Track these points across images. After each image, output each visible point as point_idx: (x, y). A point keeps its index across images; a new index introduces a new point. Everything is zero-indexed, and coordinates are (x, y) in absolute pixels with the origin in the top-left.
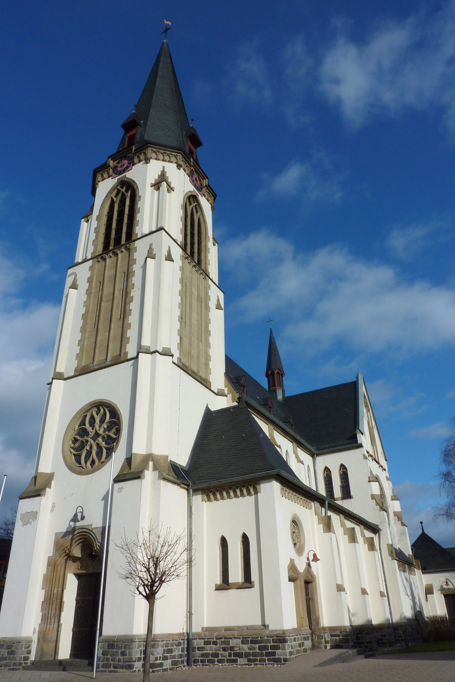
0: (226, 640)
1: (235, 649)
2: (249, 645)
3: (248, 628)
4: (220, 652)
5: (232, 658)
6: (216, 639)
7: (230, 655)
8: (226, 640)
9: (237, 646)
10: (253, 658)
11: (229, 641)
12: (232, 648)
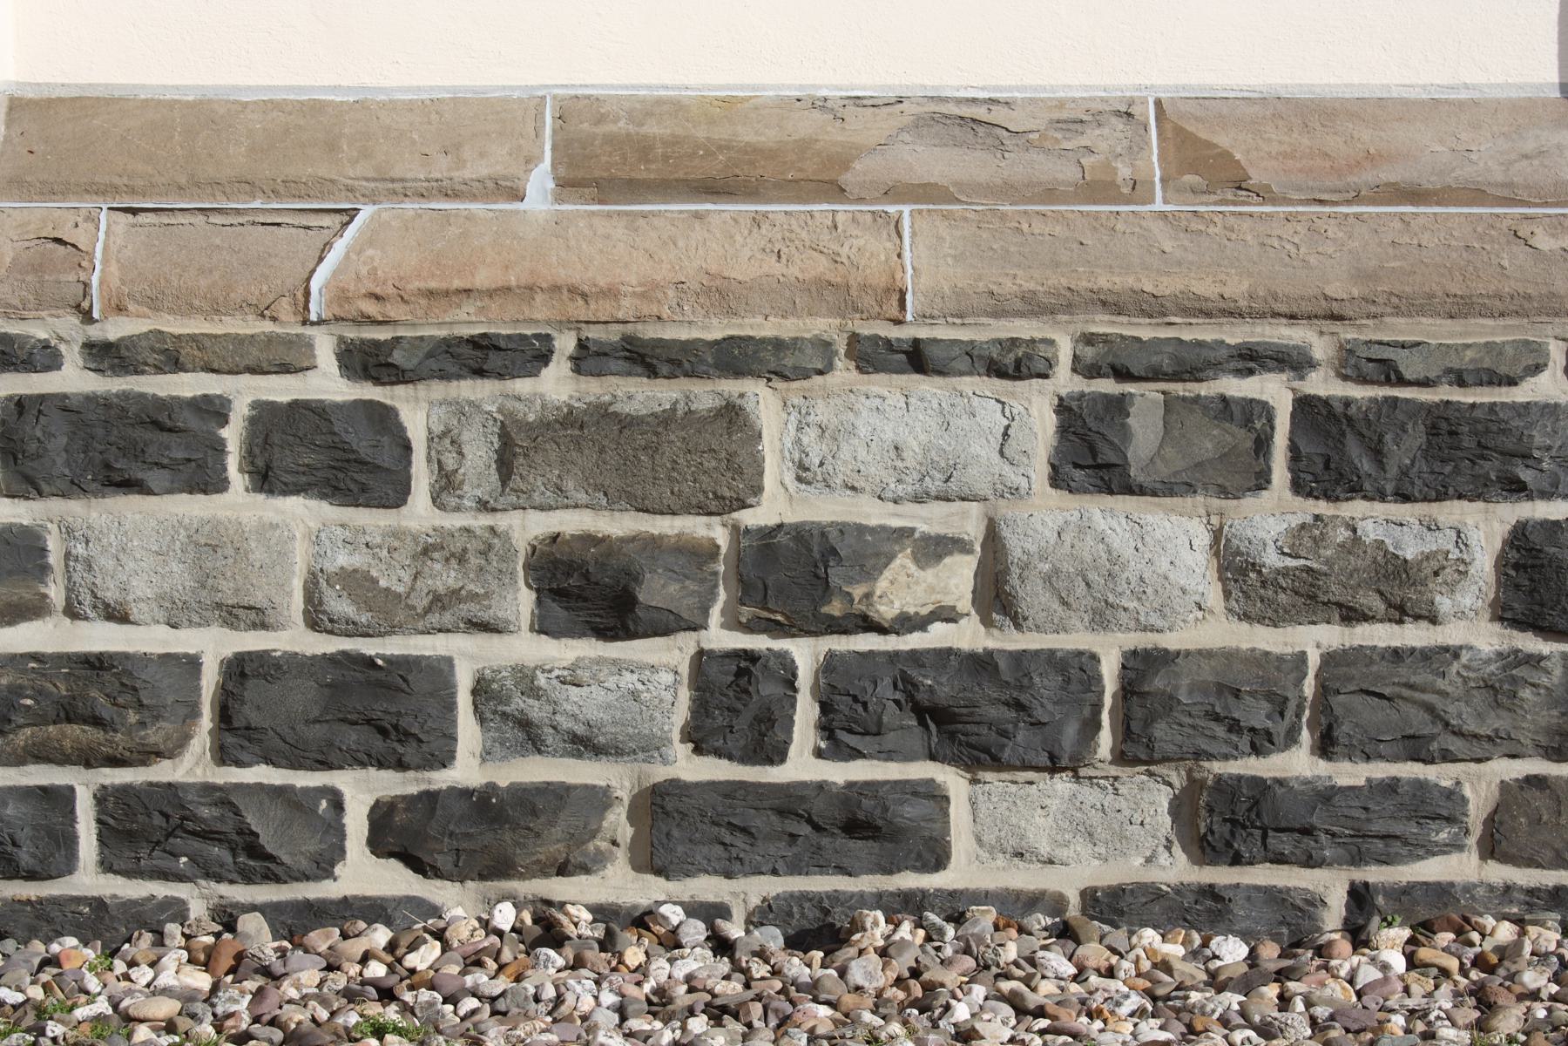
0: (642, 395)
1: (900, 587)
2: (1271, 518)
3: (1203, 150)
4: (468, 656)
5: (802, 765)
6: (365, 361)
7: (734, 704)
8: (664, 401)
9: (929, 519)
10: (1350, 774)
11: (732, 415)
12: (799, 575)
